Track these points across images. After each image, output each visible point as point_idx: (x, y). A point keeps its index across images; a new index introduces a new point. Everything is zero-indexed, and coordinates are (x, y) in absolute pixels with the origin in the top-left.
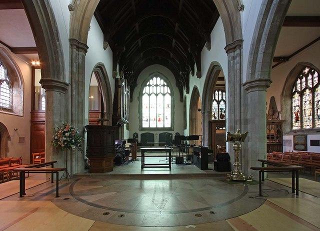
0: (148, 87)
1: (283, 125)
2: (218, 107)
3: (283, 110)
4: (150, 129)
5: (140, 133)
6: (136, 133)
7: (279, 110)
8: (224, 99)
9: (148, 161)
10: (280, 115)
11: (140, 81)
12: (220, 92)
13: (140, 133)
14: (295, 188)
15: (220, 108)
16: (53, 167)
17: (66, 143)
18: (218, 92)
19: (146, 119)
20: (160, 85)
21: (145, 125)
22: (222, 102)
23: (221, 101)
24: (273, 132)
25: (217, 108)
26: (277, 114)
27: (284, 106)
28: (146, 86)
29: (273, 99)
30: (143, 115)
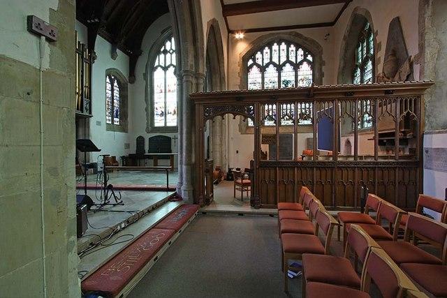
0: (162, 56)
1: (426, 98)
2: (279, 77)
3: (428, 51)
4: (166, 129)
5: (147, 137)
6: (140, 137)
7: (413, 51)
8: (293, 59)
9: (172, 206)
10: (417, 68)
11: (146, 45)
12: (283, 46)
13: (147, 137)
14: (187, 224)
15: (282, 79)
16: (86, 192)
17: (291, 274)
18: (279, 44)
19: (160, 113)
20: (171, 51)
21: (159, 122)
22: (288, 68)
23: (284, 64)
24: (389, 126)
25: (276, 80)
26: (406, 66)
27: (429, 37)
28: (159, 53)
29: (396, 24)
30: (156, 106)
